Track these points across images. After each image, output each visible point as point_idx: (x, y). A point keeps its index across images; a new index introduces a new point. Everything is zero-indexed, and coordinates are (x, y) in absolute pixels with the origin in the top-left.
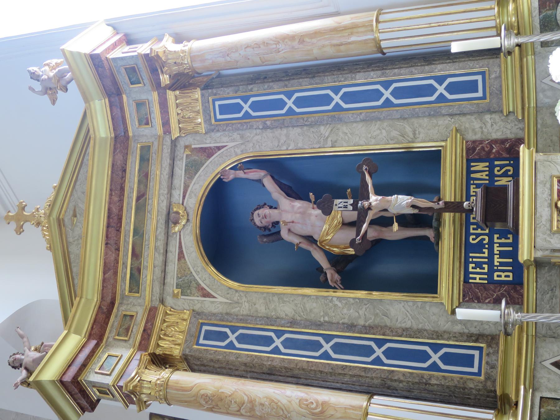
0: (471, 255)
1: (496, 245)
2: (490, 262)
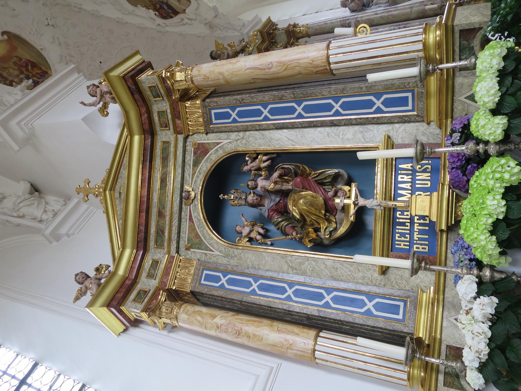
0: (397, 227)
1: (416, 225)
2: (411, 234)
